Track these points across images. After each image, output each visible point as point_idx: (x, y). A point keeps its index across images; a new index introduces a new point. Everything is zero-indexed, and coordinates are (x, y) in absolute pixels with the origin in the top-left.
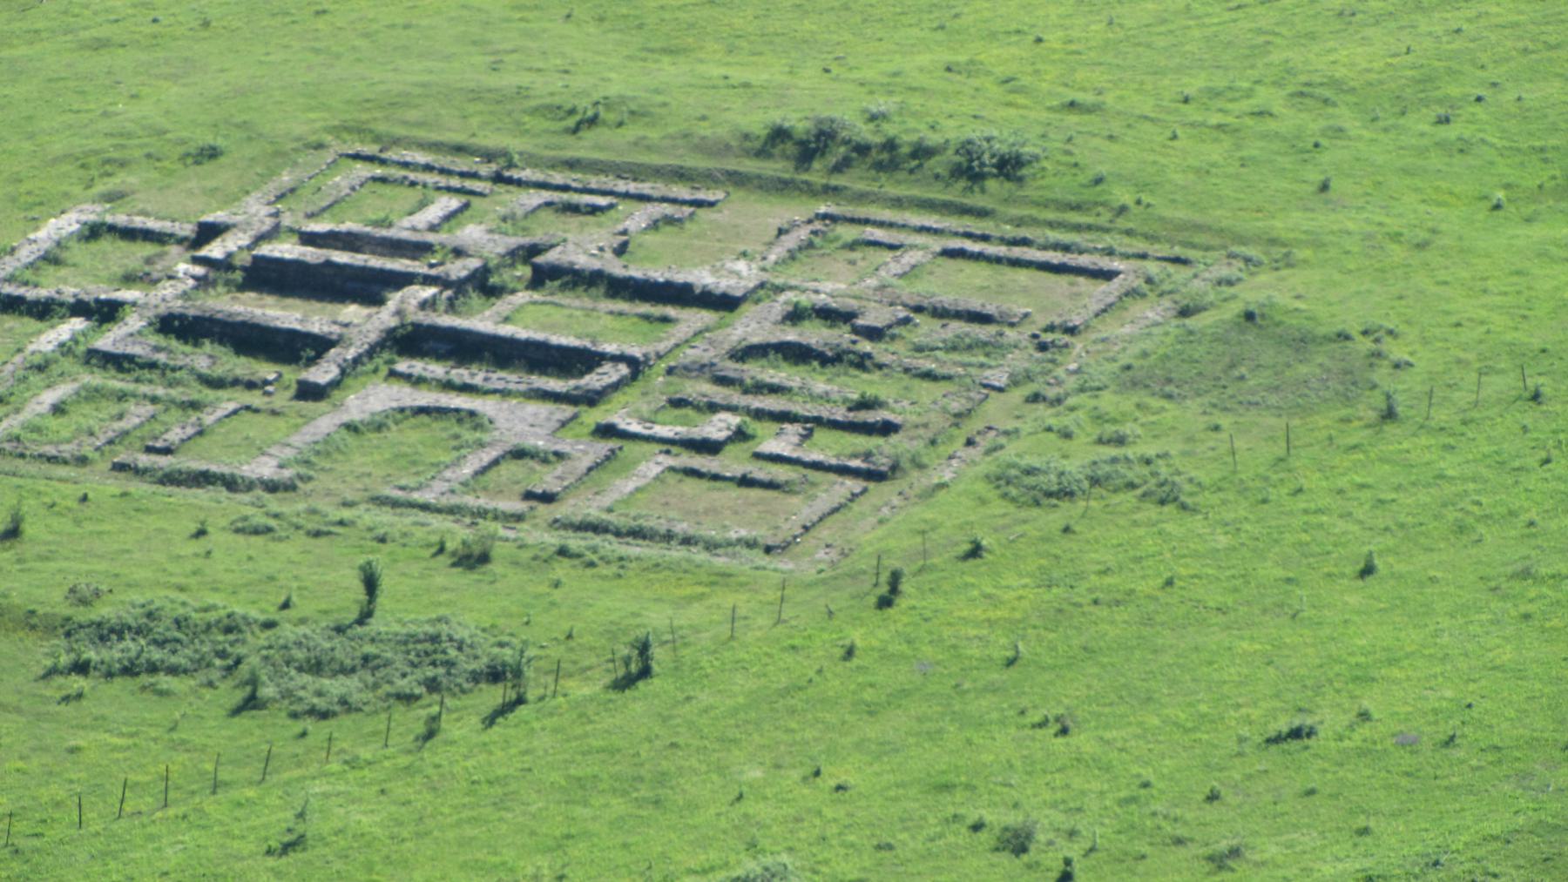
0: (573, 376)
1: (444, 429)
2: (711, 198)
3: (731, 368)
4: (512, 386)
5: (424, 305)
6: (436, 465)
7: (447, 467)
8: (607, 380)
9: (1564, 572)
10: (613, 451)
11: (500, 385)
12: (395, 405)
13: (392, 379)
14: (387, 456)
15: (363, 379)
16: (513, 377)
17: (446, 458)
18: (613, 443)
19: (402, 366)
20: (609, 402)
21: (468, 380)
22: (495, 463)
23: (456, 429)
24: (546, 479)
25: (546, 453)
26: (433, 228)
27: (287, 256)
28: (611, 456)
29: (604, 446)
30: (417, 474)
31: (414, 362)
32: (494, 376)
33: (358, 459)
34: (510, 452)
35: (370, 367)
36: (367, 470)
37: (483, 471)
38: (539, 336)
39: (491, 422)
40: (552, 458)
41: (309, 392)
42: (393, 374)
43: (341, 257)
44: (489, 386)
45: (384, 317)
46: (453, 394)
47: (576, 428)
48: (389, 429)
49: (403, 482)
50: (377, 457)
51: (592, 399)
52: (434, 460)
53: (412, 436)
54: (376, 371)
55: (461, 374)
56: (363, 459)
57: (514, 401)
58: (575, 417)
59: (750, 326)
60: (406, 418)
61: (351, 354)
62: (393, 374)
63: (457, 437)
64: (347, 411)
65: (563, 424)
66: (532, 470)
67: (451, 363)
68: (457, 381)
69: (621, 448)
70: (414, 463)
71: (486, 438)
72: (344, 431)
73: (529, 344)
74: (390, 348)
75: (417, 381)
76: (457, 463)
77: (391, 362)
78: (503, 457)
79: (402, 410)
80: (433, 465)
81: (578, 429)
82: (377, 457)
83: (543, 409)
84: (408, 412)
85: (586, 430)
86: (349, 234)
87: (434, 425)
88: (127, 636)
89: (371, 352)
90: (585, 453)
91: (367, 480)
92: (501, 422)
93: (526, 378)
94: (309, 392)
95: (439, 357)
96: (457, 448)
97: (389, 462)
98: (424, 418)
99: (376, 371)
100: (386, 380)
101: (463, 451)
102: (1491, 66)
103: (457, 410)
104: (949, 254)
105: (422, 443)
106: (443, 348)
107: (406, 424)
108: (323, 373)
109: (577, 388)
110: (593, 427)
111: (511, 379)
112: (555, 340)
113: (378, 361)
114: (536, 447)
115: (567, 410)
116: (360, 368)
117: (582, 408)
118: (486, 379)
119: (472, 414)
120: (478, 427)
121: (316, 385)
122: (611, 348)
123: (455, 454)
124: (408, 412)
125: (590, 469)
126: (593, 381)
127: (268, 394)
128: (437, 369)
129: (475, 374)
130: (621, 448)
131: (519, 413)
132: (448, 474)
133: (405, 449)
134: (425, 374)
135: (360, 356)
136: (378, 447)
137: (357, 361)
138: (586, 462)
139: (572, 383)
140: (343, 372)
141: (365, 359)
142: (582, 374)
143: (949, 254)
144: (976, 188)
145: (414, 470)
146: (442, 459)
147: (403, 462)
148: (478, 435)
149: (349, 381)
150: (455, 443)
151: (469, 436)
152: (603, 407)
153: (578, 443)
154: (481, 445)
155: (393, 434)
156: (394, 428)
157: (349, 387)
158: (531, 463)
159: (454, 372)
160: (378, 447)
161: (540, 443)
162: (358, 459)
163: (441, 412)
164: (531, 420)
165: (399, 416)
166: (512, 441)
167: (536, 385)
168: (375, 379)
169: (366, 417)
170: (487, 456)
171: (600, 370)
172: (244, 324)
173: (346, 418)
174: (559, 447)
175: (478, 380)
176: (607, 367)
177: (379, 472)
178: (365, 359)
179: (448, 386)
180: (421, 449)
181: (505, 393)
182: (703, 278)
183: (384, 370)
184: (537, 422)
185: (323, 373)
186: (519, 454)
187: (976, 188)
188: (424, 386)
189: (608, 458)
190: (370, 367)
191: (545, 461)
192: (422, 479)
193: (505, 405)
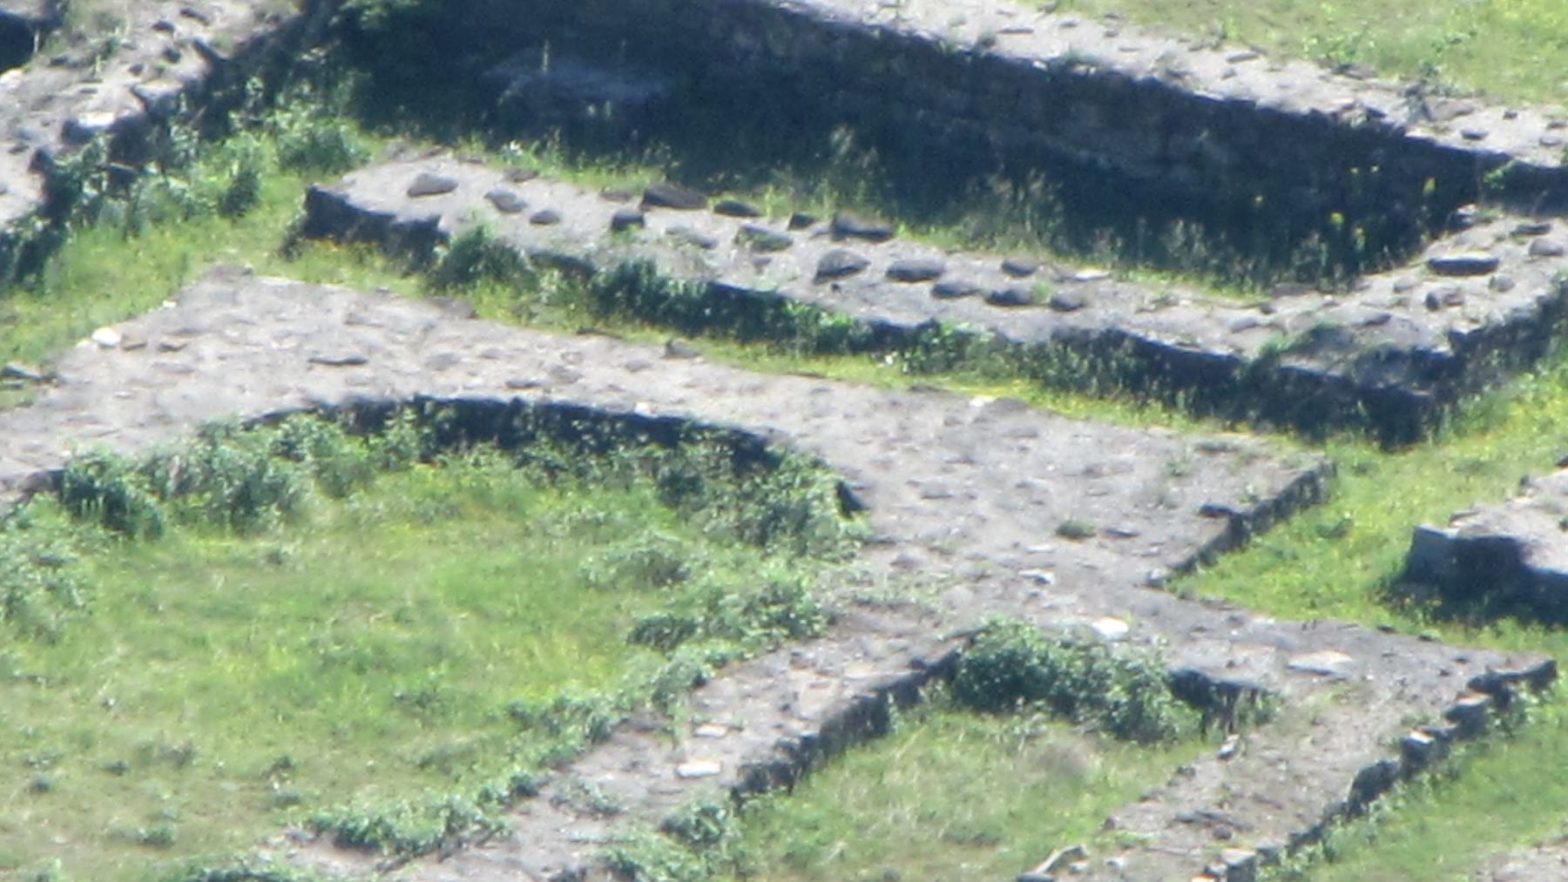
0: (1308, 278)
1: (591, 530)
4: (970, 318)
6: (548, 722)
7: (599, 736)
8: (1482, 305)
9: (1566, 555)
10: (1495, 687)
11: (905, 308)
12: (331, 387)
13: (326, 252)
14: (281, 662)
15: (166, 241)
16: (980, 269)
17: (595, 687)
18: (1504, 648)
19: (383, 181)
20: (1490, 420)
21: (737, 273)
22: (864, 722)
23: (659, 534)
25: (1137, 684)
28: (1490, 711)
29: (1448, 663)
30: (438, 765)
31: (446, 166)
32: (879, 257)
33: (118, 670)
34: (946, 668)
35: (208, 178)
36: (168, 732)
37: (795, 765)
38: (1135, 52)
39: (849, 503)
40: (1167, 709)
42: (330, 221)
44: (850, 308)
46: (649, 343)
47: (1299, 558)
48: (292, 512)
49: (364, 807)
50: (227, 667)
51: (1399, 401)
52: (526, 697)
53: (420, 554)
54: (239, 200)
55: (696, 240)
56: (142, 678)
57: (982, 398)
58: (1302, 495)
60: (394, 461)
61: (107, 100)
62: (330, 221)
63: (661, 572)
64: (75, 411)
65: (1238, 530)
66: (1065, 772)
67: (644, 178)
68: (675, 273)
69: (1542, 678)
70: (421, 705)
71: (818, 584)
72: (50, 518)
73: (1067, 86)
74: (324, 80)
75: (460, 267)
76: (654, 716)
77: (321, 156)
78: (906, 693)
79: (369, 417)
80: (520, 718)
81: (1316, 564)
82: (227, 667)
83: (1139, 445)
84: (401, 431)
85: (1360, 573)
87: (545, 505)
89: (222, 94)
90: (1354, 692)
91: (159, 785)
92: (897, 508)
93: (1047, 273)
95: (587, 143)
96: (660, 636)
97: (289, 696)
98: (488, 466)
99: (239, 200)
100: (289, 250)
101: (688, 653)
103: (669, 431)
105: (470, 601)
106: (610, 93)
107: (384, 495)
109: (1319, 338)
110: (1398, 549)
111: (969, 273)
112: (1212, 75)
113: (252, 146)
114: (1087, 647)
115: (1268, 459)
116: (152, 182)
117: (1350, 450)
118: (830, 272)
119: (748, 453)
120: (783, 525)
122: (1516, 133)
123: (646, 666)
124: (401, 431)
125: (1371, 784)
126: (1402, 304)
128: (570, 206)
129: (774, 242)
130: (1542, 678)
131: (1003, 461)
132: (602, 774)
133: (371, 629)
134: (499, 228)
135: (157, 114)
136: (232, 612)
137: (136, 141)
138: (1356, 742)
139: (1298, 309)
140: (59, 198)
141: (182, 137)
142: (1350, 266)
144: (75, 746)
145: (425, 743)
146: (576, 692)
147: (362, 700)
148: (774, 568)
149: (89, 249)
150: (651, 607)
151: (723, 570)
152: (1457, 450)
153: (1312, 635)
154: (790, 621)
155: (309, 539)
156: (321, 508)
157: (87, 282)
158: (1057, 735)
159: (660, 221)
160: (232, 612)
161: (1110, 628)
162: (118, 670)
163: (577, 434)
164: (1065, 502)
165: (351, 449)
166: (961, 612)
167: (1096, 318)
168: (229, 243)
169: (180, 445)
170: (825, 682)
171: (1446, 249)
173: (63, 447)
174: (1207, 657)
175: (790, 272)
176: (1489, 234)
177: (234, 751)
178: (182, 137)
179: (626, 299)
180: (461, 626)
181: (929, 352)
183: (283, 200)
184: (1099, 514)
186: (992, 682)
187: (75, 746)
188: (491, 297)
189: (1467, 723)
190: (208, 178)
191: (1133, 727)
192: (463, 797)
193: (930, 418)
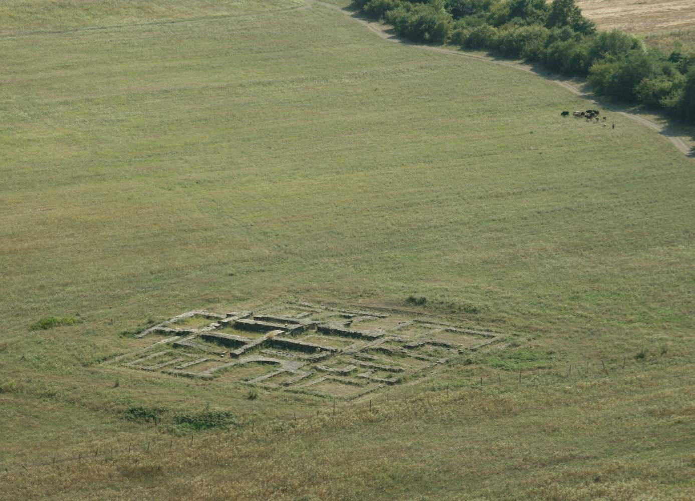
2: (384, 316)
3: (360, 354)
5: (279, 335)
24: (289, 379)
26: (300, 318)
27: (251, 323)
41: (234, 356)
43: (259, 322)
45: (264, 337)
59: (375, 344)
86: (268, 318)
88: (569, 457)
94: (234, 356)
102: (446, 295)
104: (447, 331)
108: (237, 352)
121: (235, 354)
127: (222, 357)
139: (311, 356)
143: (447, 331)
163: (268, 362)
172: (222, 338)
182: (366, 332)
185: (237, 352)
